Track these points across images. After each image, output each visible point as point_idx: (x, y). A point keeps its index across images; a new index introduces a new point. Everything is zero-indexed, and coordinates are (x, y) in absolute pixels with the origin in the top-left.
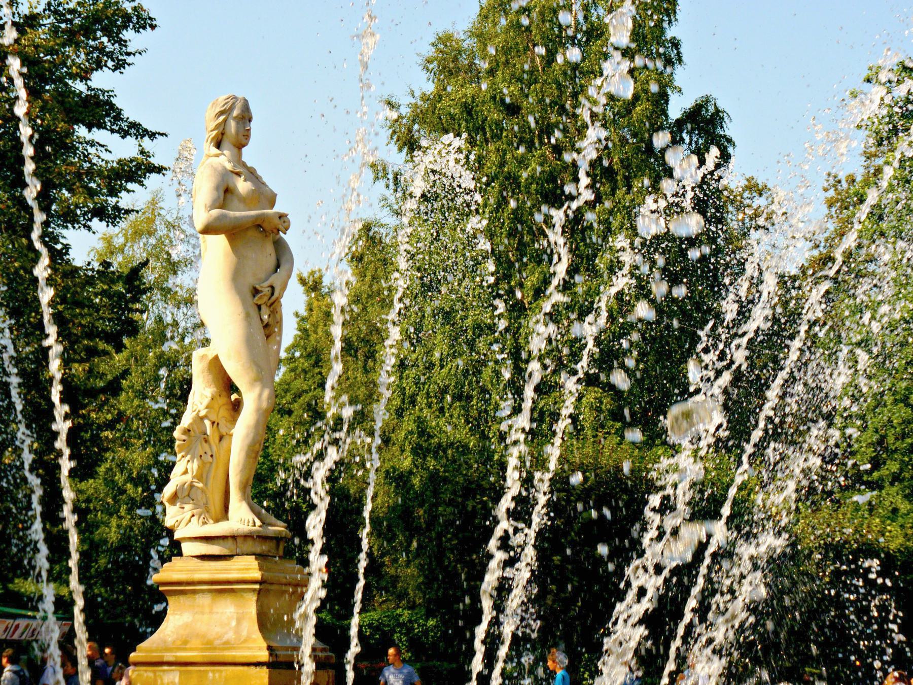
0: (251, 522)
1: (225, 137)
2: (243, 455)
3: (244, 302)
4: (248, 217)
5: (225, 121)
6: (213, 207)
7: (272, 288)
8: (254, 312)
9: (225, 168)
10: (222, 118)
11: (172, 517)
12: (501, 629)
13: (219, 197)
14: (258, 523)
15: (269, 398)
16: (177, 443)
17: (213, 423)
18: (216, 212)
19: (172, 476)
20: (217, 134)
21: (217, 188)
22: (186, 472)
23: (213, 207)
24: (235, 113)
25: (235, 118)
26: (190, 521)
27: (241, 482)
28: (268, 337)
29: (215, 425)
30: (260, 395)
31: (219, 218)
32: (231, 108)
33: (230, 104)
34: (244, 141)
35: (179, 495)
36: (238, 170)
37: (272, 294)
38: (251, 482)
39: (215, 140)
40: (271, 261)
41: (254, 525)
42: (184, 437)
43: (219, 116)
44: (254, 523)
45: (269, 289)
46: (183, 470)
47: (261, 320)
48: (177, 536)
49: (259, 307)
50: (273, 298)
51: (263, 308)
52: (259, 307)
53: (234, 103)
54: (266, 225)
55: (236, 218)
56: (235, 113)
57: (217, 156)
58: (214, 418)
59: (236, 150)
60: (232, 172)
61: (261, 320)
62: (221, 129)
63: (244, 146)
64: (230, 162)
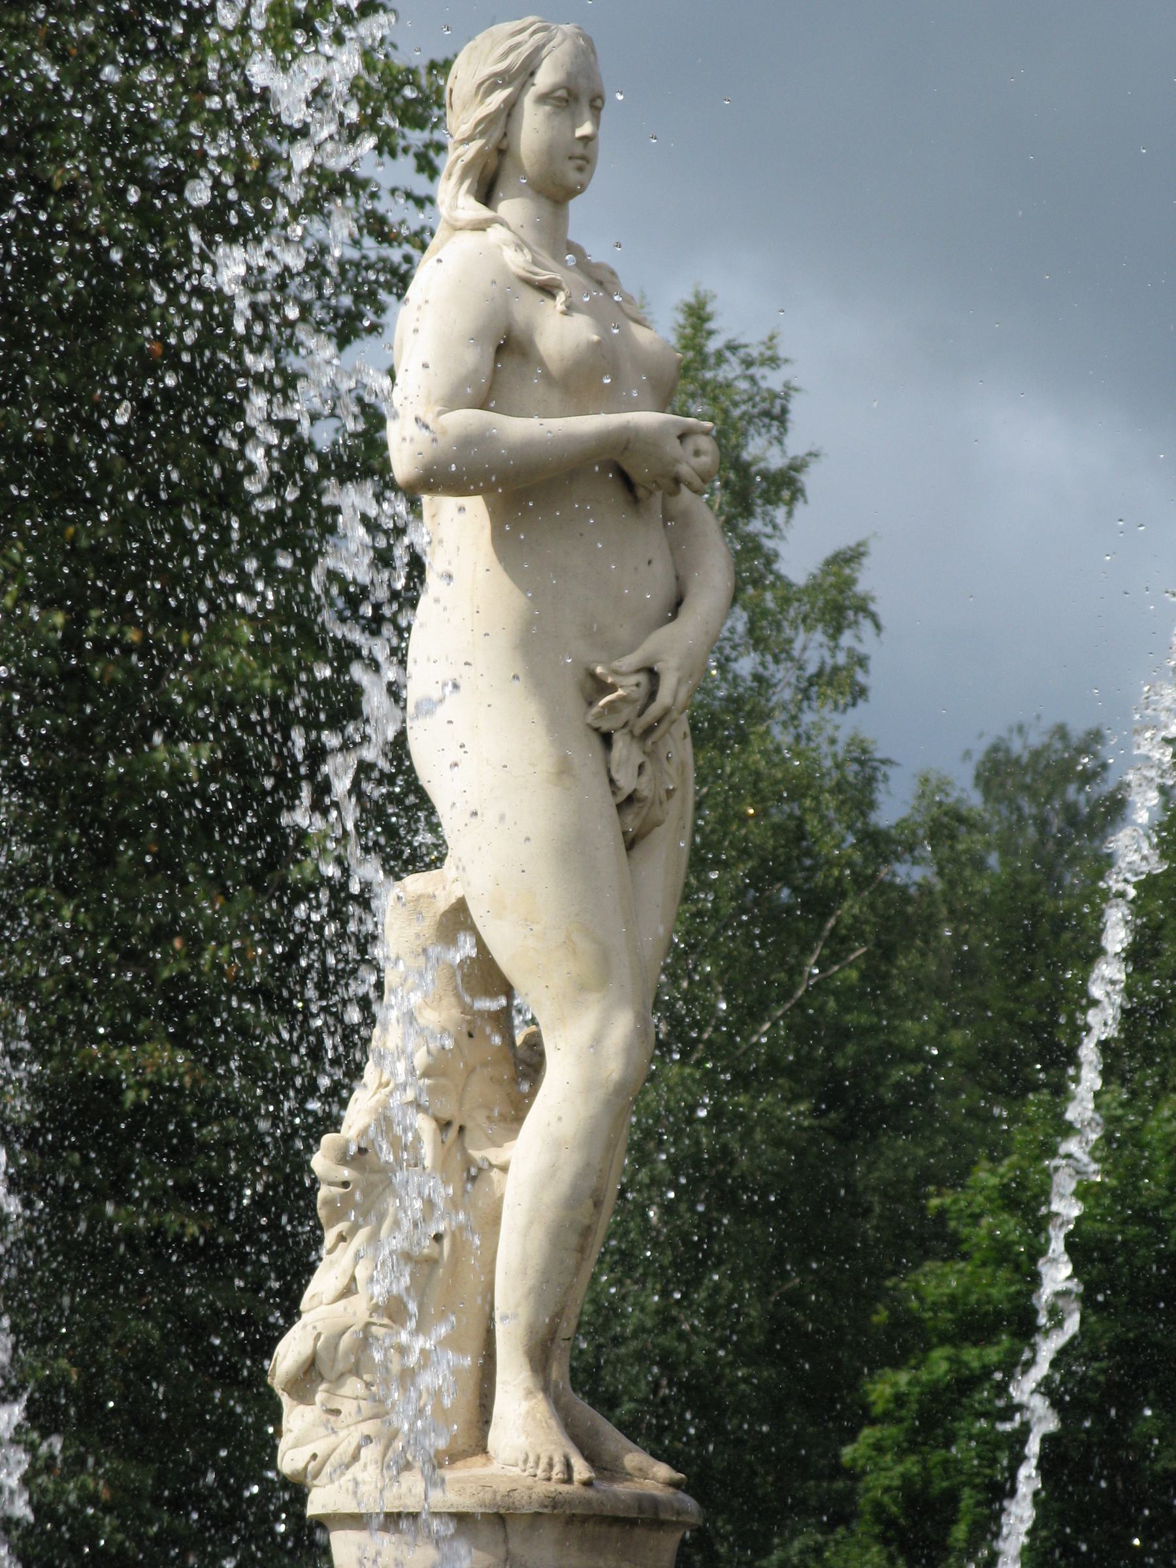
0: (558, 1468)
1: (508, 163)
2: (538, 1240)
3: (555, 724)
4: (571, 439)
5: (510, 109)
6: (452, 402)
7: (653, 675)
8: (587, 754)
9: (504, 268)
10: (499, 97)
11: (295, 1446)
12: (323, 336)
13: (476, 371)
14: (582, 1472)
15: (629, 1050)
16: (323, 1192)
17: (444, 1125)
18: (466, 419)
19: (304, 1304)
20: (480, 153)
21: (477, 338)
22: (349, 1290)
23: (452, 402)
24: (545, 78)
25: (543, 99)
26: (355, 1457)
27: (531, 1330)
28: (631, 843)
29: (453, 1132)
30: (597, 1041)
31: (467, 442)
32: (528, 70)
33: (525, 50)
34: (573, 176)
35: (324, 1366)
36: (544, 276)
37: (652, 695)
38: (567, 1328)
39: (476, 172)
40: (654, 595)
41: (569, 1480)
42: (346, 1173)
43: (489, 91)
44: (568, 1467)
45: (642, 678)
46: (341, 1283)
47: (612, 781)
48: (314, 1507)
49: (606, 739)
50: (655, 709)
51: (620, 743)
52: (606, 739)
53: (538, 49)
54: (640, 473)
55: (529, 445)
56: (545, 78)
57: (480, 226)
58: (448, 1110)
59: (547, 207)
60: (528, 282)
61: (612, 781)
62: (497, 134)
63: (572, 192)
64: (520, 246)
